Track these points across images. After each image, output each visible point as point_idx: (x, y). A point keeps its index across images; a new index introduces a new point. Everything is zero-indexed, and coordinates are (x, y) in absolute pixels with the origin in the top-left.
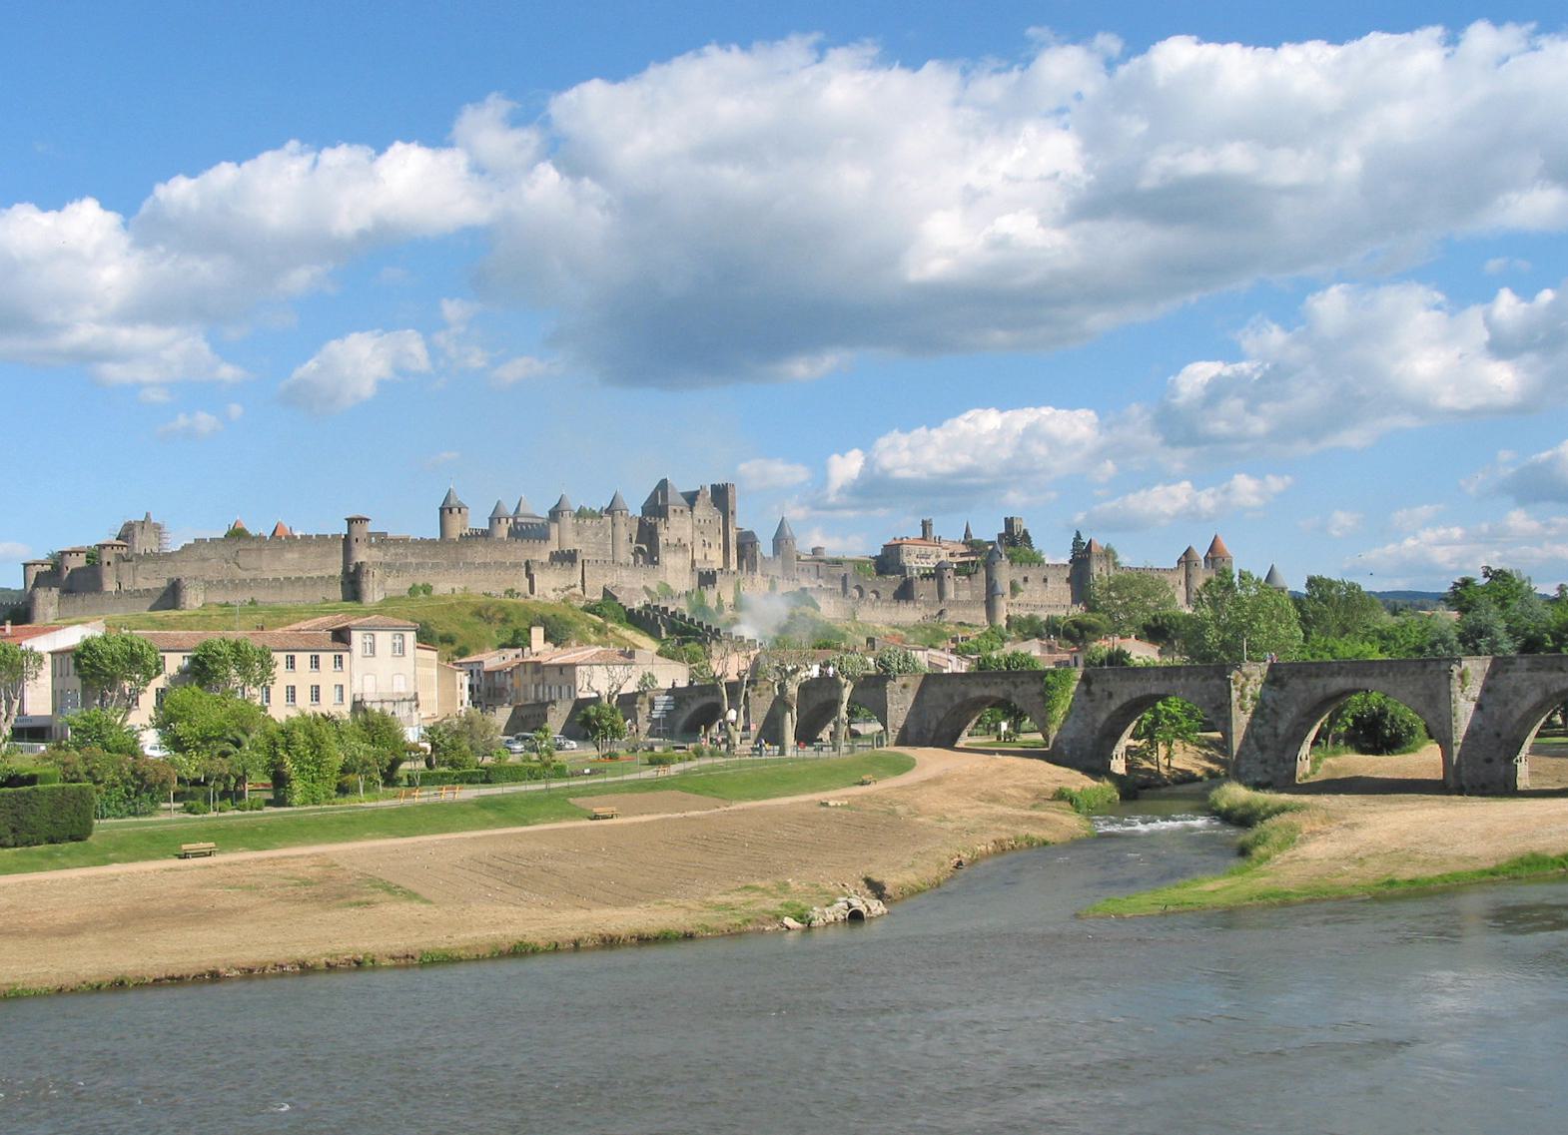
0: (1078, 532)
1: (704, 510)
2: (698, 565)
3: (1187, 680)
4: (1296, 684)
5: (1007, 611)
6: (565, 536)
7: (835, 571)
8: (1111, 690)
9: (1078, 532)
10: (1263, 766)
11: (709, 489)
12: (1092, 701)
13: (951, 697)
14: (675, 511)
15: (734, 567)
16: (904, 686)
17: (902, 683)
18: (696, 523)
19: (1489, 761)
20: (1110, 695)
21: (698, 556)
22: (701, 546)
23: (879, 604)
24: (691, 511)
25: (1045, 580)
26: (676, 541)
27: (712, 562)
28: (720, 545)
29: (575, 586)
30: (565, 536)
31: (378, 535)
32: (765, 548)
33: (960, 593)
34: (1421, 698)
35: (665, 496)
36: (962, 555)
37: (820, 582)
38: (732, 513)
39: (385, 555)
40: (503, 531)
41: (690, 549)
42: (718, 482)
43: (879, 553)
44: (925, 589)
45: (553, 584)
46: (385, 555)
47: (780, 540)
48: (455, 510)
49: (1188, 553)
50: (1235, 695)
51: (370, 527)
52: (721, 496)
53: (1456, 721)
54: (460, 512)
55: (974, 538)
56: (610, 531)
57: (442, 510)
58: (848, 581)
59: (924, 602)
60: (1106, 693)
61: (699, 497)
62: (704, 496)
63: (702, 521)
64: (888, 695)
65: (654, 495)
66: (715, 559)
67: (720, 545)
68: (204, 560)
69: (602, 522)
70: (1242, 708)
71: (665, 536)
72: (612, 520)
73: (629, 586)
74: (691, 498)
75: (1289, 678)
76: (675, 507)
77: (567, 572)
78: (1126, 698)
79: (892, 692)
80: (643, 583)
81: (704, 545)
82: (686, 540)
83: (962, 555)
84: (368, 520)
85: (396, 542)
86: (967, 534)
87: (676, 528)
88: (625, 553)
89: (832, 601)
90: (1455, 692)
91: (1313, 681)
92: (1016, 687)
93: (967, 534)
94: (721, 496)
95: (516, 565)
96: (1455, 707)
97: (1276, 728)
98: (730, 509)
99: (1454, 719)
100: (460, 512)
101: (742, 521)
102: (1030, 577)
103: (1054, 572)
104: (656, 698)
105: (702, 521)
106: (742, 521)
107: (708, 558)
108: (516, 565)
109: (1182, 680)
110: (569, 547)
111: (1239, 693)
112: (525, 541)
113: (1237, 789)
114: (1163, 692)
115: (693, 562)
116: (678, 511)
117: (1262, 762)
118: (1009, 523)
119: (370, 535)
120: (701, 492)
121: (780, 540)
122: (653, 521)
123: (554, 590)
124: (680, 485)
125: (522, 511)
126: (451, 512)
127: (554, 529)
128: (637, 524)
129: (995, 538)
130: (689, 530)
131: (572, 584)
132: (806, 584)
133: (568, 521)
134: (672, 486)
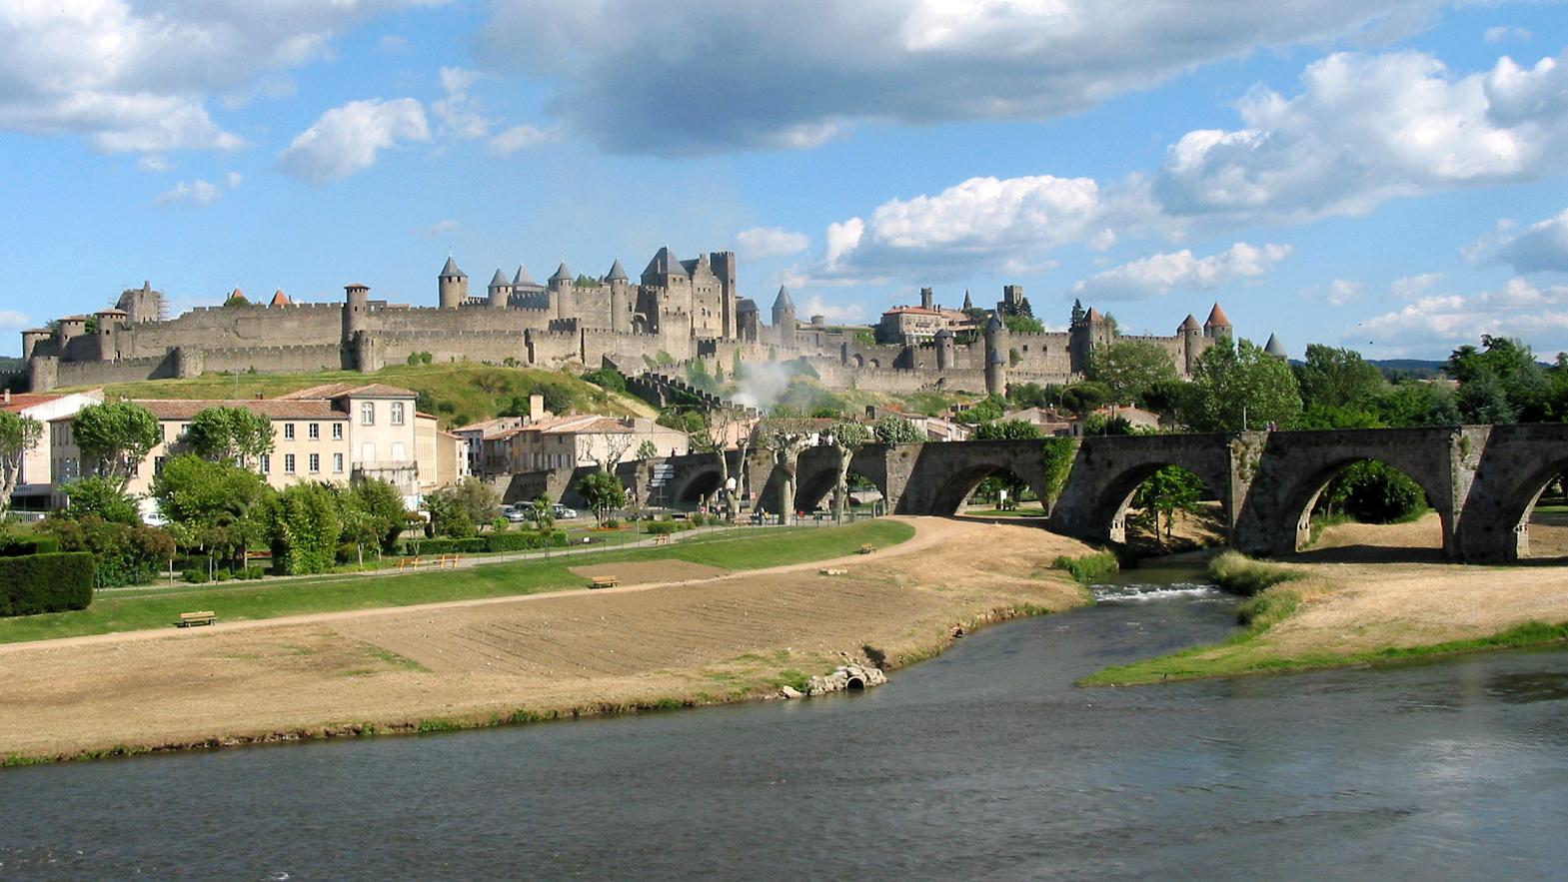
0: (1078, 301)
1: (704, 279)
3: (1187, 448)
4: (1296, 452)
6: (565, 305)
7: (834, 339)
9: (1078, 301)
11: (708, 258)
15: (733, 335)
16: (904, 455)
18: (696, 291)
20: (1110, 464)
21: (698, 324)
22: (701, 314)
25: (1045, 349)
29: (574, 355)
30: (565, 305)
31: (377, 303)
32: (765, 316)
33: (960, 362)
35: (664, 265)
36: (962, 323)
37: (820, 350)
40: (502, 299)
41: (690, 318)
42: (719, 250)
43: (879, 322)
44: (924, 358)
45: (553, 353)
47: (780, 309)
48: (455, 279)
50: (1235, 463)
51: (370, 296)
52: (720, 264)
53: (1456, 490)
54: (459, 281)
55: (973, 306)
57: (441, 279)
58: (848, 350)
59: (924, 370)
60: (1106, 462)
61: (699, 266)
62: (703, 264)
63: (702, 290)
65: (653, 264)
66: (715, 327)
70: (1242, 476)
71: (664, 304)
74: (691, 267)
78: (1125, 467)
79: (891, 461)
80: (643, 352)
82: (685, 308)
83: (962, 323)
84: (367, 289)
85: (395, 310)
86: (967, 303)
87: (675, 297)
88: (624, 321)
89: (831, 370)
90: (1455, 462)
92: (1016, 455)
93: (967, 303)
94: (720, 264)
95: (515, 334)
97: (1275, 497)
98: (730, 277)
99: (1454, 488)
100: (459, 281)
101: (742, 289)
102: (1030, 346)
103: (1054, 340)
104: (656, 467)
105: (702, 290)
106: (742, 289)
108: (515, 334)
110: (568, 315)
111: (1239, 462)
118: (1009, 291)
119: (369, 303)
121: (780, 309)
122: (652, 289)
124: (680, 253)
126: (450, 281)
127: (553, 298)
129: (995, 307)
130: (688, 299)
132: (805, 353)
133: (567, 289)
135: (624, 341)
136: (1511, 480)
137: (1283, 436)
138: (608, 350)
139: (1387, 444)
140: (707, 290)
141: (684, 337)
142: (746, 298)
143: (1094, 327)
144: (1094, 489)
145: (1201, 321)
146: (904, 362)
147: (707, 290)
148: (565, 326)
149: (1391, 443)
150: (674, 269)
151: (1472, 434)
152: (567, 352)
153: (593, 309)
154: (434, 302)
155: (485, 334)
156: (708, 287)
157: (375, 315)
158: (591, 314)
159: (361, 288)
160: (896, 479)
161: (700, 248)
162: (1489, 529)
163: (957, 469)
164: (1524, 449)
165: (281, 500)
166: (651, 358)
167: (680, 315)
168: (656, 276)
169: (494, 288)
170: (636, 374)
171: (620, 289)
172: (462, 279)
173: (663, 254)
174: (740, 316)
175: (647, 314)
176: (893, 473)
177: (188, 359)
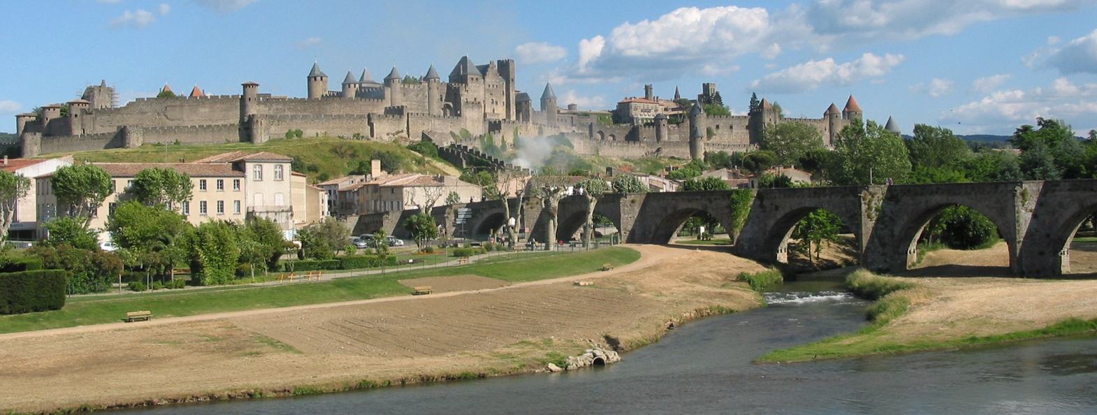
0: (754, 95)
1: (492, 78)
2: (488, 117)
3: (830, 197)
5: (704, 149)
7: (584, 121)
9: (754, 95)
11: (496, 64)
12: (764, 212)
13: (665, 209)
15: (513, 118)
16: (633, 202)
21: (488, 110)
22: (490, 103)
23: (615, 144)
25: (731, 127)
26: (473, 100)
27: (498, 114)
29: (402, 131)
30: (397, 96)
31: (264, 95)
32: (535, 105)
33: (672, 136)
35: (465, 69)
36: (673, 110)
37: (574, 128)
38: (512, 80)
40: (352, 93)
41: (483, 106)
42: (503, 58)
43: (615, 109)
45: (387, 130)
46: (269, 109)
48: (319, 78)
49: (831, 108)
50: (864, 207)
52: (504, 68)
54: (322, 79)
55: (681, 97)
57: (309, 78)
59: (647, 142)
61: (489, 69)
65: (457, 68)
66: (501, 112)
70: (869, 216)
72: (428, 86)
74: (484, 70)
76: (472, 76)
77: (397, 122)
78: (788, 210)
80: (450, 130)
81: (493, 103)
82: (480, 99)
83: (673, 110)
84: (257, 85)
85: (277, 100)
86: (677, 95)
87: (473, 91)
88: (437, 108)
92: (711, 202)
93: (677, 95)
94: (504, 68)
95: (361, 117)
96: (1018, 217)
97: (893, 231)
99: (1017, 224)
100: (322, 79)
101: (519, 85)
104: (459, 210)
107: (495, 112)
108: (361, 117)
109: (827, 197)
110: (398, 104)
111: (867, 206)
114: (814, 206)
115: (485, 115)
116: (474, 79)
117: (883, 255)
118: (706, 87)
119: (259, 95)
120: (491, 66)
124: (476, 61)
125: (365, 78)
126: (315, 80)
127: (388, 92)
129: (696, 98)
130: (482, 93)
132: (564, 130)
133: (397, 86)
135: (437, 122)
138: (427, 127)
140: (495, 86)
141: (478, 119)
143: (766, 112)
145: (840, 108)
146: (633, 136)
147: (495, 86)
150: (472, 72)
151: (1030, 187)
155: (339, 117)
156: (495, 84)
157: (262, 104)
160: (627, 219)
161: (490, 57)
167: (476, 104)
168: (459, 76)
169: (346, 84)
170: (446, 145)
171: (434, 85)
172: (323, 78)
173: (464, 61)
174: (518, 104)
175: (453, 103)
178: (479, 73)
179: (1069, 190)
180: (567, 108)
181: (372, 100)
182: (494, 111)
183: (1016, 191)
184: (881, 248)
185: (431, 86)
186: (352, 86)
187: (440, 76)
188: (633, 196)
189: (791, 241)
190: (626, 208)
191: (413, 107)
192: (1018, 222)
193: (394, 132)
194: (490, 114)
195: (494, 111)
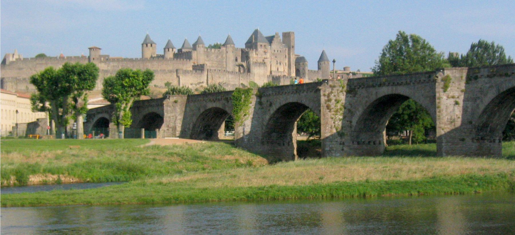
2: (273, 74)
3: (307, 93)
4: (362, 92)
6: (199, 57)
8: (271, 101)
10: (341, 146)
11: (281, 35)
12: (263, 108)
14: (261, 46)
16: (176, 102)
17: (173, 100)
18: (273, 52)
19: (463, 140)
20: (271, 105)
21: (274, 69)
24: (270, 45)
27: (281, 72)
28: (286, 63)
29: (203, 83)
30: (199, 57)
31: (104, 56)
34: (428, 99)
35: (256, 38)
38: (293, 47)
39: (108, 66)
40: (170, 55)
42: (287, 30)
45: (191, 82)
46: (108, 66)
48: (149, 45)
50: (323, 99)
51: (102, 53)
52: (287, 37)
53: (439, 112)
54: (151, 46)
56: (225, 55)
57: (165, 49)
60: (269, 103)
61: (275, 39)
62: (278, 38)
63: (276, 51)
64: (165, 108)
67: (286, 63)
68: (20, 69)
69: (221, 50)
70: (328, 107)
71: (253, 56)
73: (233, 83)
74: (270, 40)
75: (358, 88)
76: (261, 44)
77: (199, 76)
79: (167, 106)
81: (277, 63)
84: (100, 49)
85: (114, 60)
88: (231, 66)
90: (439, 92)
91: (371, 89)
94: (287, 37)
95: (171, 71)
96: (439, 103)
97: (351, 122)
98: (292, 45)
99: (437, 110)
100: (151, 46)
101: (299, 51)
105: (276, 51)
106: (299, 51)
108: (171, 71)
109: (305, 93)
110: (201, 62)
111: (326, 98)
112: (182, 60)
113: (355, 167)
116: (263, 45)
117: (340, 144)
119: (101, 56)
123: (191, 84)
124: (266, 33)
125: (185, 45)
126: (147, 46)
127: (194, 55)
128: (241, 52)
131: (201, 81)
133: (201, 49)
134: (260, 32)
135: (230, 76)
136: (478, 105)
137: (355, 82)
139: (409, 84)
140: (279, 52)
142: (301, 56)
144: (263, 120)
147: (279, 52)
148: (199, 68)
149: (412, 84)
151: (452, 73)
152: (199, 81)
153: (216, 60)
154: (140, 56)
156: (279, 49)
157: (103, 62)
158: (214, 62)
159: (96, 48)
160: (169, 117)
162: (463, 140)
163: (202, 110)
164: (486, 83)
165: (498, 175)
166: (246, 85)
172: (153, 45)
173: (256, 33)
176: (167, 113)
177: (8, 84)
178: (267, 41)
179: (488, 76)
180: (343, 69)
181: (185, 60)
182: (278, 69)
183: (437, 77)
184: (339, 138)
185: (227, 50)
186: (171, 50)
187: (235, 43)
188: (175, 98)
189: (303, 137)
190: (169, 109)
191: (214, 65)
192: (438, 107)
193: (196, 83)
194: (275, 72)
195: (278, 69)
